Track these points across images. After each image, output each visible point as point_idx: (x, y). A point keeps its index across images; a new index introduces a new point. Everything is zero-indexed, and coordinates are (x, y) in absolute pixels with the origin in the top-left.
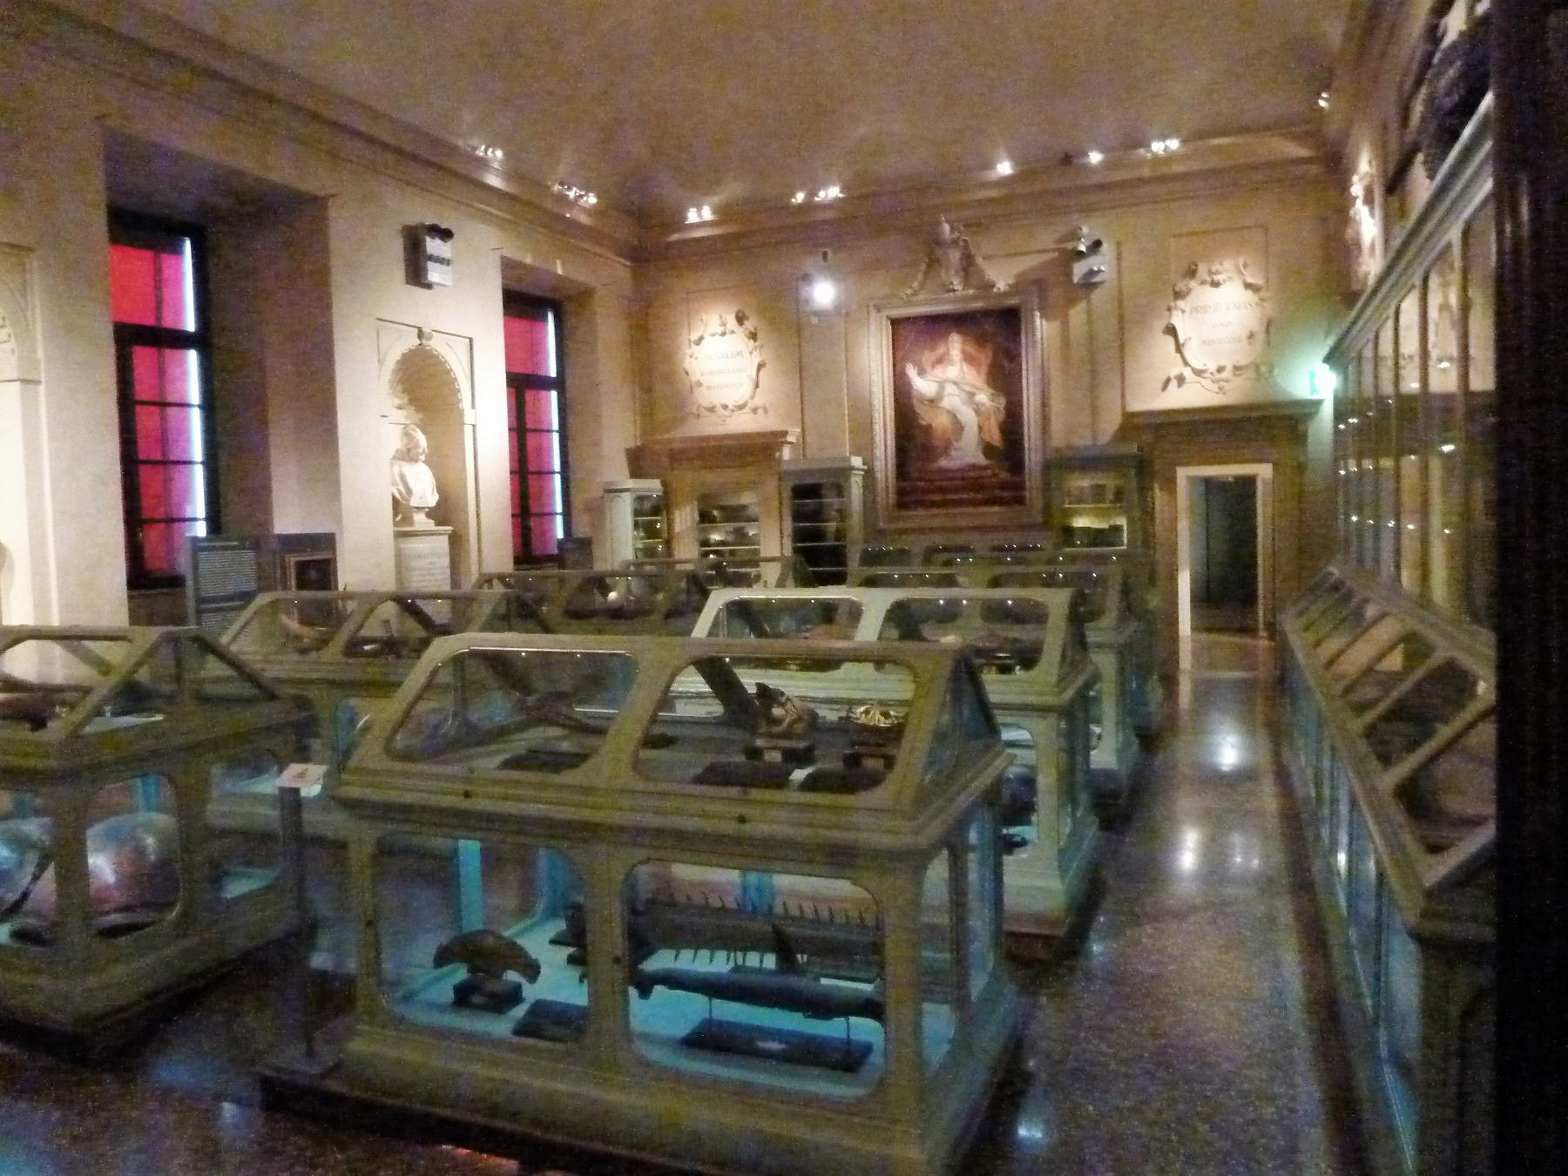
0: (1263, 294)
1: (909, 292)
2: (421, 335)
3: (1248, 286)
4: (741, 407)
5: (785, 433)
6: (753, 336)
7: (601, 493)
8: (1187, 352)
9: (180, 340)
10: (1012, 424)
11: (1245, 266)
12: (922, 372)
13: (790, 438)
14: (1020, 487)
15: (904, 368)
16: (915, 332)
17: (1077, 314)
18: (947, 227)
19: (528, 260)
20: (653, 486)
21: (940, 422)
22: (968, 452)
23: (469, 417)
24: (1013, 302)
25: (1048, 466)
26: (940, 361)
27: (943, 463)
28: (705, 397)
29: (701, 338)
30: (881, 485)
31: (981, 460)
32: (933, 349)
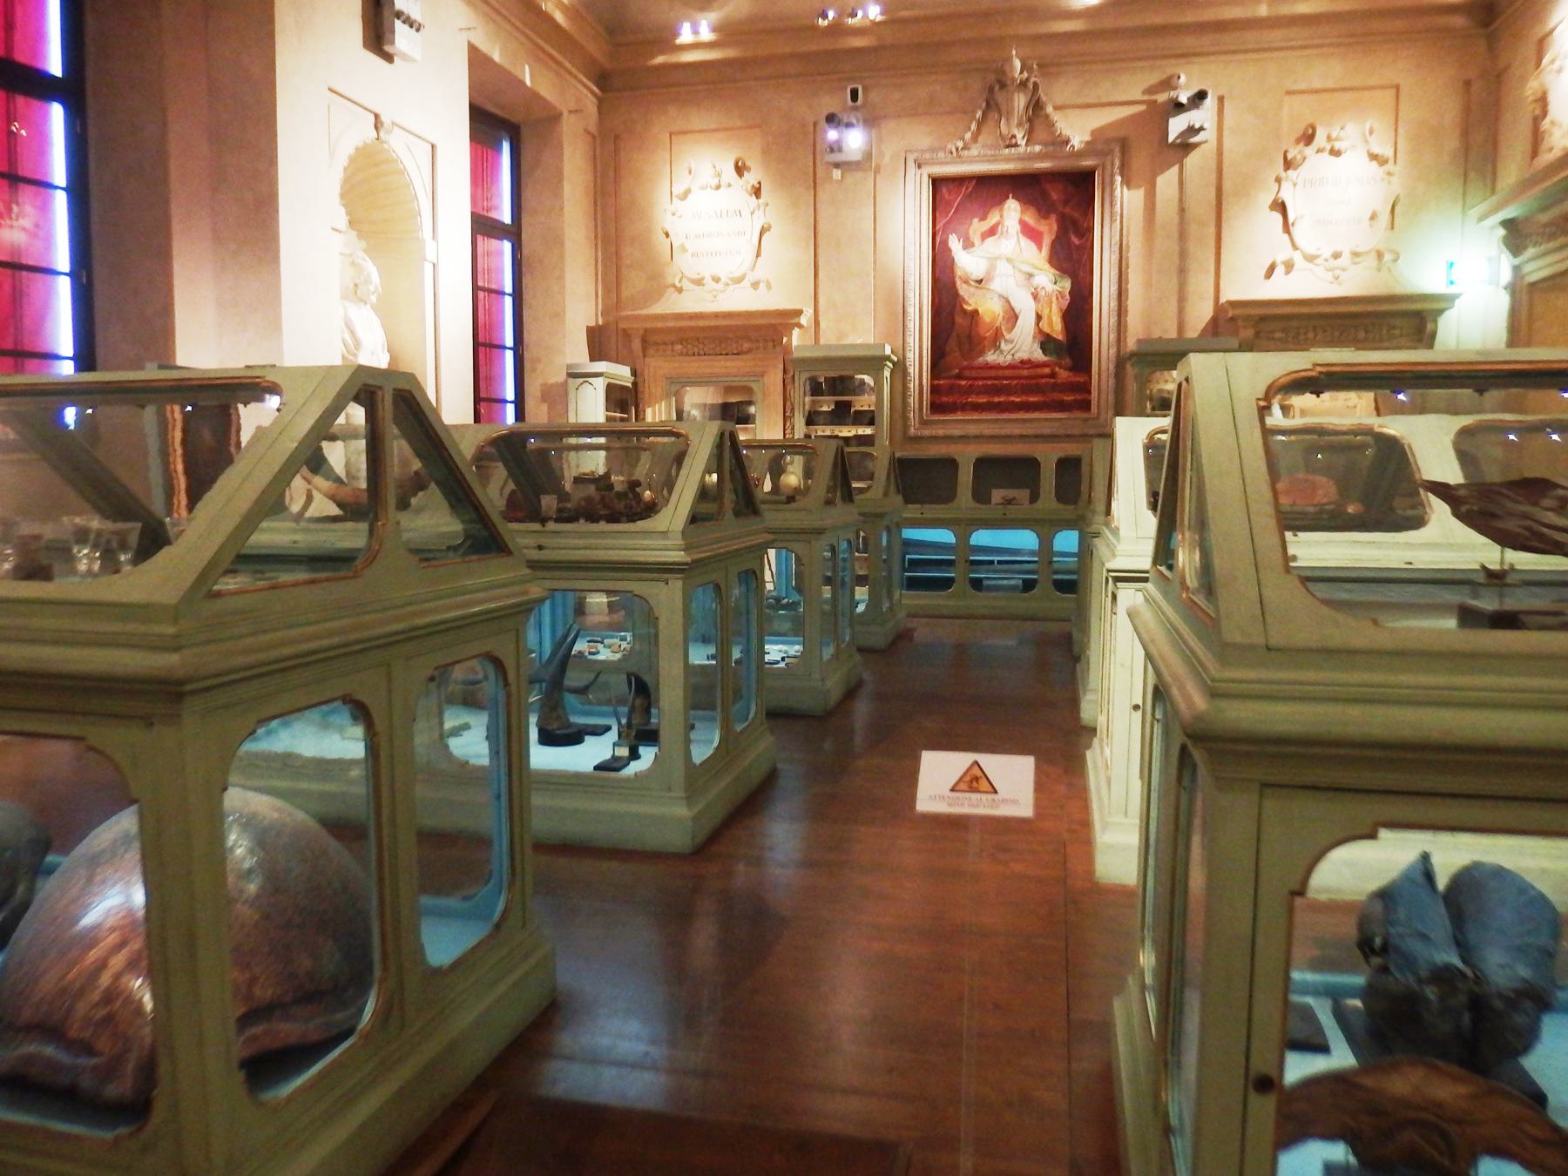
0: (1390, 166)
1: (960, 144)
2: (378, 124)
3: (1373, 157)
4: (739, 280)
5: (799, 313)
6: (757, 192)
7: (561, 377)
8: (1295, 231)
9: (43, 87)
10: (1078, 310)
11: (1371, 132)
12: (968, 245)
13: (803, 320)
14: (1086, 388)
15: (945, 243)
16: (960, 197)
17: (1167, 182)
18: (1017, 64)
19: (496, 57)
20: (622, 373)
21: (988, 306)
22: (1022, 344)
23: (430, 254)
24: (1088, 163)
25: (1121, 363)
26: (992, 232)
27: (991, 357)
28: (685, 265)
29: (687, 193)
30: (913, 386)
31: (1039, 355)
32: (983, 218)
